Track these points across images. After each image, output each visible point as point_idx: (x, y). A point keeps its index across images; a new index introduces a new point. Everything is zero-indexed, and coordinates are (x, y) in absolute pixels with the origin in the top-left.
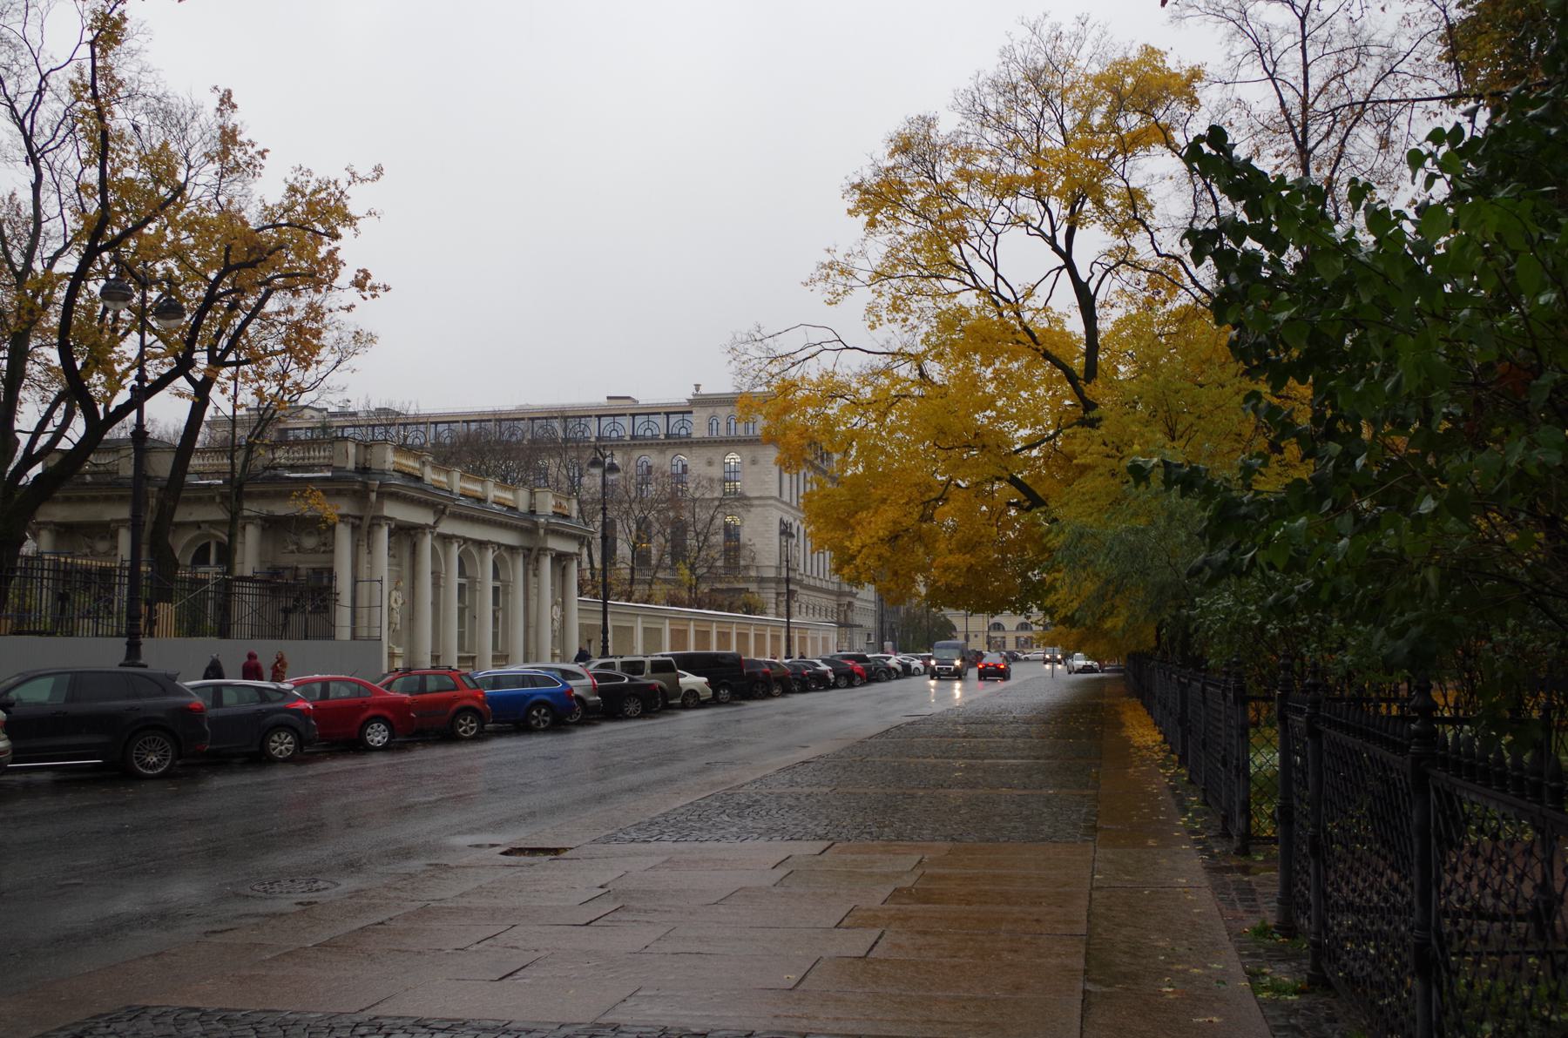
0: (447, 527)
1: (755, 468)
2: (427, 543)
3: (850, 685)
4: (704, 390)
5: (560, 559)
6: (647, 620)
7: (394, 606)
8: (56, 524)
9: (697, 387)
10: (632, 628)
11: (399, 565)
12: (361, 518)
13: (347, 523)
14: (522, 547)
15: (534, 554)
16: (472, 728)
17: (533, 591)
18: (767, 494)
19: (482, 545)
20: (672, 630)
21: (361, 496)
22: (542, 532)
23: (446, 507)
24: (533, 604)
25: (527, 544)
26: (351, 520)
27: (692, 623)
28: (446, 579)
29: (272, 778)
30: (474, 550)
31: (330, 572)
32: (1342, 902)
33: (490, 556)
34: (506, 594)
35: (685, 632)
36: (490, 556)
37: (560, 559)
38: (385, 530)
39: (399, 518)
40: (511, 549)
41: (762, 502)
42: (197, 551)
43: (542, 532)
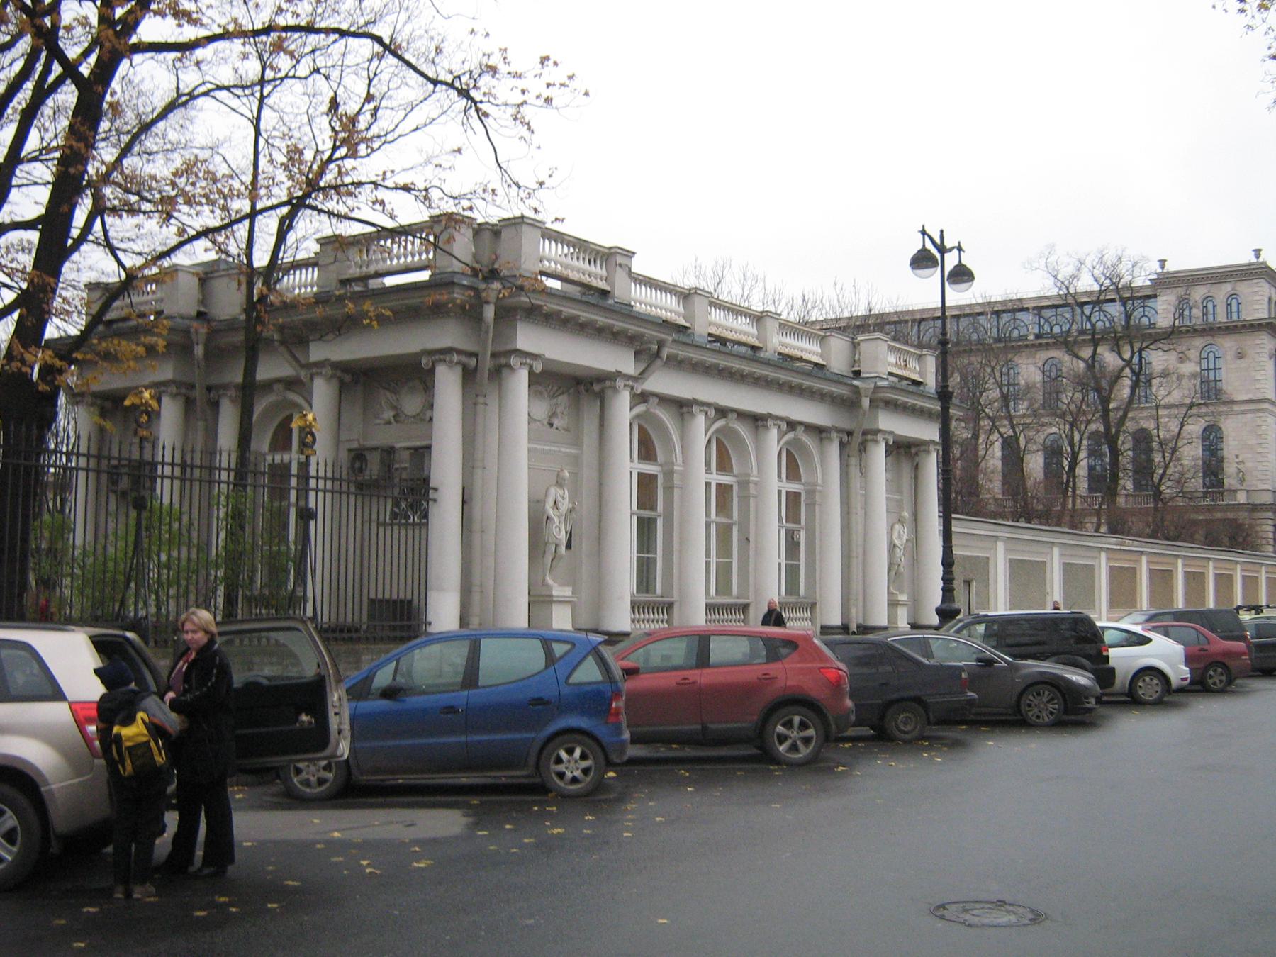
0: (665, 383)
1: (1242, 364)
2: (623, 409)
3: (1226, 689)
4: (1171, 267)
5: (903, 450)
6: (1069, 551)
7: (897, 542)
8: (96, 395)
9: (1162, 263)
10: (1134, 569)
11: (900, 492)
12: (850, 433)
13: (451, 364)
14: (839, 430)
15: (857, 438)
16: (807, 741)
17: (857, 502)
18: (1260, 396)
19: (757, 421)
20: (1111, 569)
21: (850, 404)
22: (866, 402)
23: (661, 344)
24: (858, 519)
25: (845, 424)
26: (456, 358)
27: (1180, 562)
28: (684, 475)
29: (944, 734)
30: (742, 430)
31: (422, 453)
32: (1197, 312)
33: (773, 440)
34: (811, 506)
35: (1133, 572)
36: (773, 440)
37: (903, 450)
38: (523, 375)
39: (548, 355)
40: (819, 432)
41: (1252, 407)
42: (275, 434)
43: (866, 402)
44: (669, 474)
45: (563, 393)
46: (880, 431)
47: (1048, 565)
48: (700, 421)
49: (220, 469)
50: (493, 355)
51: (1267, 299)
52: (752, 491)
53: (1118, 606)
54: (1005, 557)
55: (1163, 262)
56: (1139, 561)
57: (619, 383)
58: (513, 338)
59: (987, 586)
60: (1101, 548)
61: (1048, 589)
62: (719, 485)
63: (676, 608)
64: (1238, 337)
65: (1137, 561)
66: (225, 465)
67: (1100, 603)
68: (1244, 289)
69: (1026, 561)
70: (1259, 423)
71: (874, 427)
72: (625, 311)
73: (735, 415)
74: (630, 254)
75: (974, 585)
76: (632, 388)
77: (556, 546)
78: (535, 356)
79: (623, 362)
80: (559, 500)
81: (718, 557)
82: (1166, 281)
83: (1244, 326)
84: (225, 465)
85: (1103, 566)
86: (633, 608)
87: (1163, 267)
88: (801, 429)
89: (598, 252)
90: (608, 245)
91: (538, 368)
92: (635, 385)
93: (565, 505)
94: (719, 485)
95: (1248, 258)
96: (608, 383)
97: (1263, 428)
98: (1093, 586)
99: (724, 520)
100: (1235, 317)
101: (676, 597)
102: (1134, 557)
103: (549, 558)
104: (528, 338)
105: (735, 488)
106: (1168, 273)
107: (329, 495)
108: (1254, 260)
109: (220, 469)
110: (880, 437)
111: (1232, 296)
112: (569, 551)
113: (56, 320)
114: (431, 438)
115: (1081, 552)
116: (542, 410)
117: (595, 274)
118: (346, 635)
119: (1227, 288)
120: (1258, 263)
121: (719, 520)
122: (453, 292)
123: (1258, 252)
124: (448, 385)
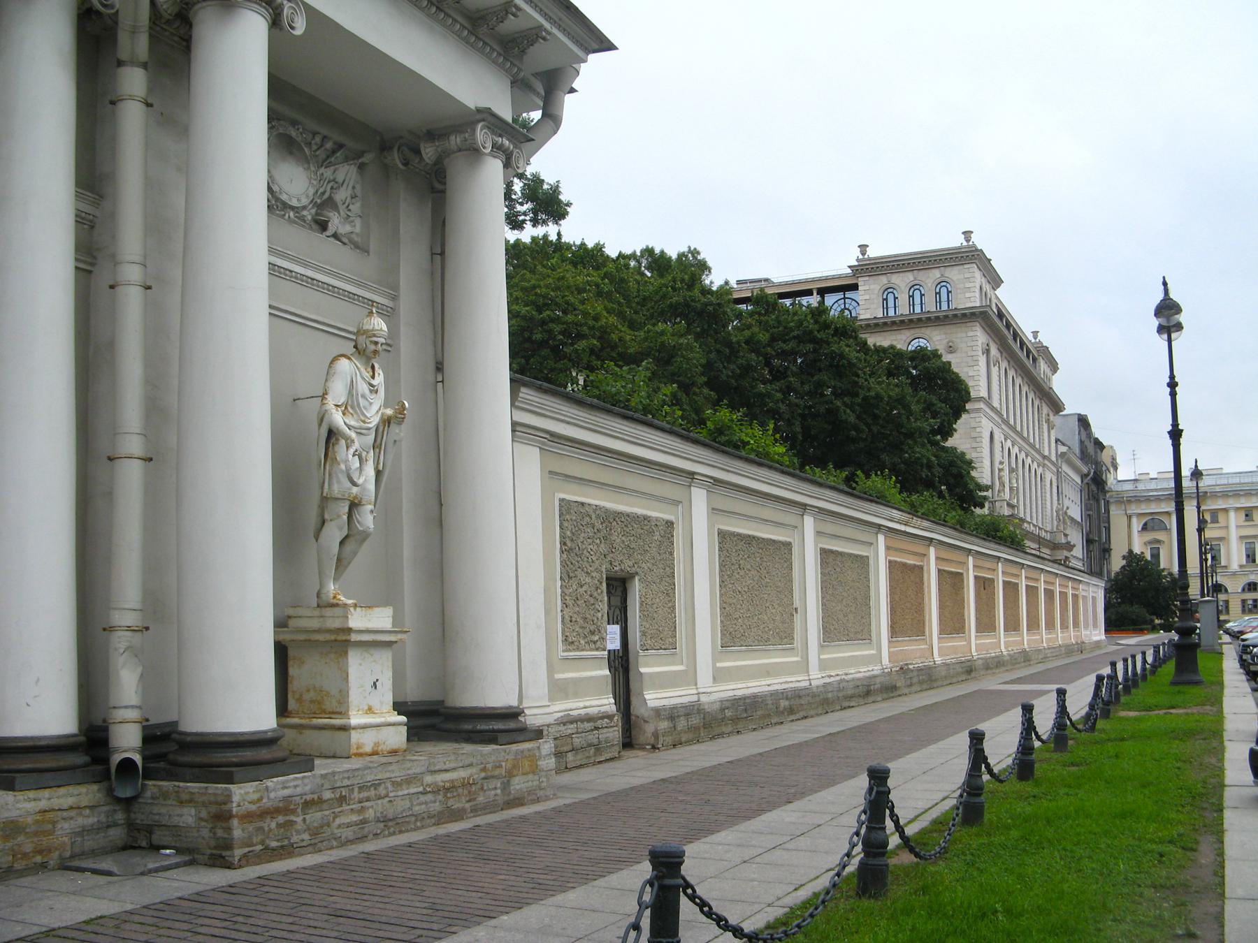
4: (872, 253)
6: (830, 528)
10: (921, 568)
35: (918, 571)
47: (795, 550)
51: (979, 288)
53: (904, 634)
55: (863, 248)
59: (670, 593)
60: (879, 527)
61: (797, 603)
64: (948, 329)
67: (930, 609)
68: (954, 274)
70: (973, 425)
75: (636, 588)
82: (869, 268)
83: (955, 316)
85: (880, 556)
87: (863, 254)
95: (957, 241)
96: (455, 141)
97: (978, 430)
98: (867, 598)
100: (944, 307)
106: (870, 259)
108: (965, 244)
111: (941, 283)
113: (860, 850)
119: (936, 274)
120: (969, 247)
123: (967, 234)
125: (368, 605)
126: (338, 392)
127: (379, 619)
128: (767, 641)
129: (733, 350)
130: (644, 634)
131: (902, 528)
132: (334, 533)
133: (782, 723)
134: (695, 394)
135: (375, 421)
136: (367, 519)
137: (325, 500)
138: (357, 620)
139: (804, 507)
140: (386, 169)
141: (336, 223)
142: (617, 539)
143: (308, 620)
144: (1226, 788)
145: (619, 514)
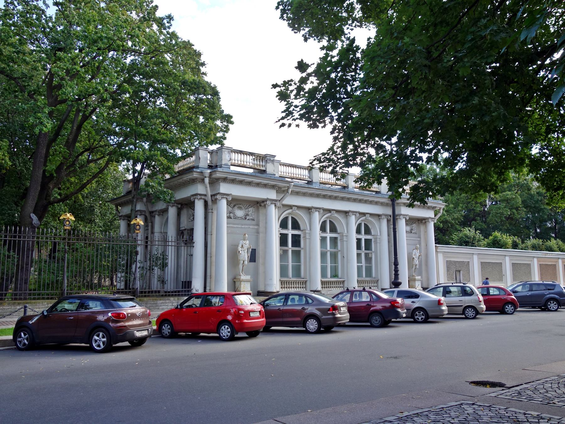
14: (386, 215)
38: (224, 202)
39: (410, 214)
44: (376, 239)
45: (251, 207)
46: (401, 215)
48: (353, 218)
49: (169, 241)
50: (211, 196)
52: (345, 239)
54: (538, 263)
56: (557, 262)
57: (430, 220)
58: (400, 210)
59: (469, 273)
62: (365, 240)
63: (308, 283)
65: (470, 258)
66: (170, 240)
69: (547, 264)
71: (400, 213)
72: (272, 177)
73: (369, 215)
74: (274, 156)
75: (461, 272)
76: (227, 199)
77: (244, 261)
78: (228, 195)
79: (272, 195)
80: (416, 254)
81: (331, 263)
84: (170, 240)
86: (358, 282)
88: (368, 216)
89: (260, 157)
90: (264, 154)
91: (230, 198)
92: (228, 197)
93: (418, 255)
94: (365, 240)
96: (427, 220)
99: (333, 250)
101: (308, 279)
102: (531, 259)
103: (414, 268)
104: (224, 188)
105: (373, 240)
107: (173, 247)
109: (169, 241)
110: (401, 217)
112: (252, 264)
114: (193, 226)
115: (523, 258)
116: (409, 228)
117: (259, 165)
118: (177, 293)
121: (332, 250)
122: (193, 175)
124: (199, 207)
125: (418, 276)
126: (414, 253)
127: (419, 277)
128: (495, 281)
129: (532, 196)
130: (463, 279)
131: (544, 256)
132: (414, 268)
133: (218, 311)
134: (519, 210)
135: (418, 256)
136: (417, 267)
137: (413, 265)
138: (417, 278)
139: (505, 255)
140: (419, 223)
141: (413, 232)
142: (457, 265)
143: (411, 277)
144: (242, 283)
145: (457, 261)
